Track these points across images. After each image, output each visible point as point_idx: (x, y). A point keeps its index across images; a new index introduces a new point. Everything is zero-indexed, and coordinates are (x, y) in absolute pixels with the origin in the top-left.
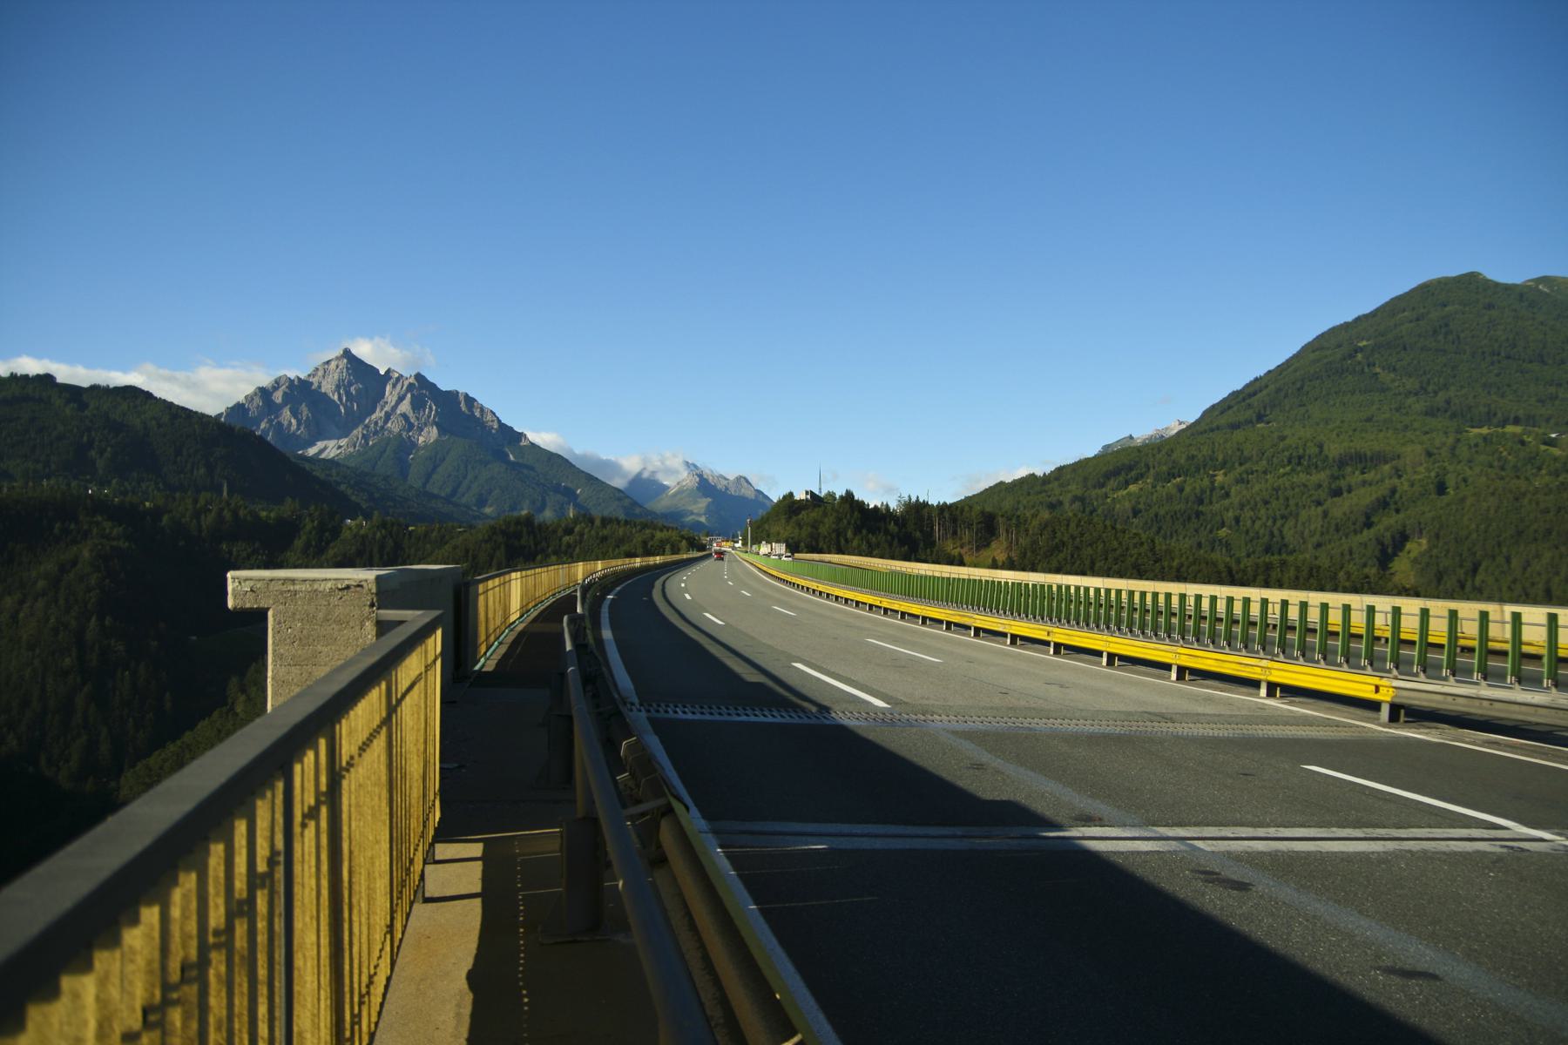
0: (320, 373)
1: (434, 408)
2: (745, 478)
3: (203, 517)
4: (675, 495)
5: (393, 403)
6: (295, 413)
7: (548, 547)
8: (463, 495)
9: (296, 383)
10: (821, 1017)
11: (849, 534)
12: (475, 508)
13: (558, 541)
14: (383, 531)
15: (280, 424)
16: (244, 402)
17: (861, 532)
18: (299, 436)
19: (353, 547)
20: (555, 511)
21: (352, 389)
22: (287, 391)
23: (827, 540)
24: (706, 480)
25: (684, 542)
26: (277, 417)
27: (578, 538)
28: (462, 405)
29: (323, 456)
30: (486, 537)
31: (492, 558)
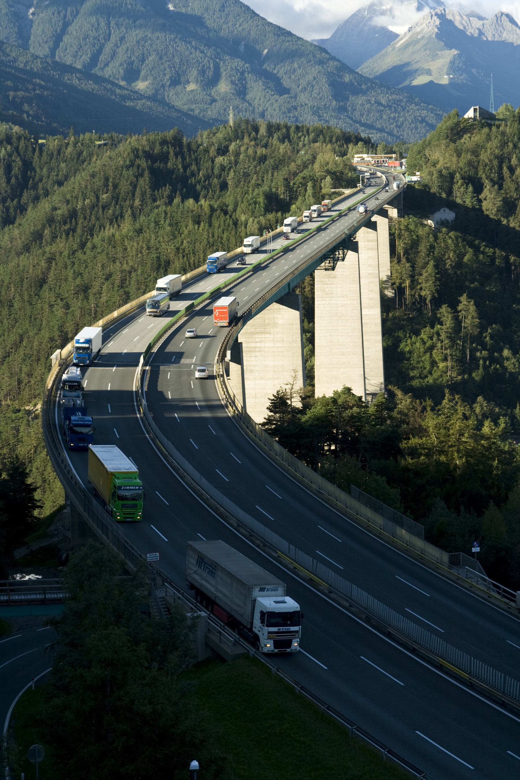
2: (508, 16)
4: (406, 46)
7: (199, 170)
8: (107, 65)
10: (247, 515)
12: (123, 83)
13: (210, 163)
14: (9, 147)
20: (233, 82)
25: (328, 178)
30: (128, 163)
31: (135, 187)
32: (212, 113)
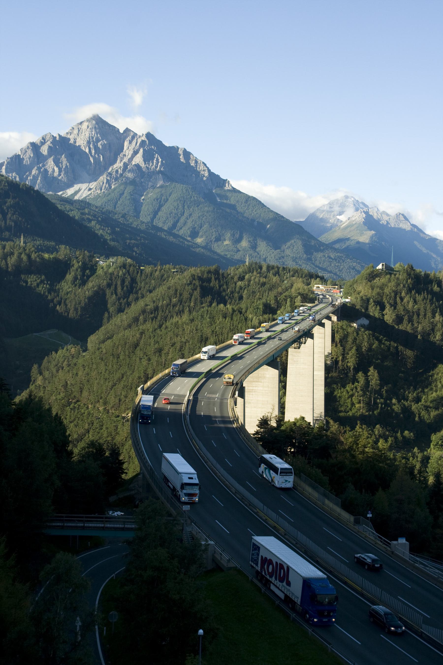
0: (76, 131)
1: (160, 160)
2: (403, 215)
3: (9, 258)
4: (346, 228)
5: (130, 156)
6: (57, 162)
7: (228, 288)
8: (181, 228)
9: (58, 139)
11: (403, 294)
12: (189, 239)
13: (234, 285)
14: (124, 270)
15: (46, 171)
16: (20, 154)
17: (411, 292)
18: (61, 180)
19: (105, 282)
20: (249, 241)
21: (99, 144)
22: (51, 145)
23: (388, 297)
24: (372, 216)
25: (299, 297)
26: (44, 165)
27: (247, 283)
28: (181, 157)
29: (76, 198)
30: (188, 282)
32: (237, 257)
